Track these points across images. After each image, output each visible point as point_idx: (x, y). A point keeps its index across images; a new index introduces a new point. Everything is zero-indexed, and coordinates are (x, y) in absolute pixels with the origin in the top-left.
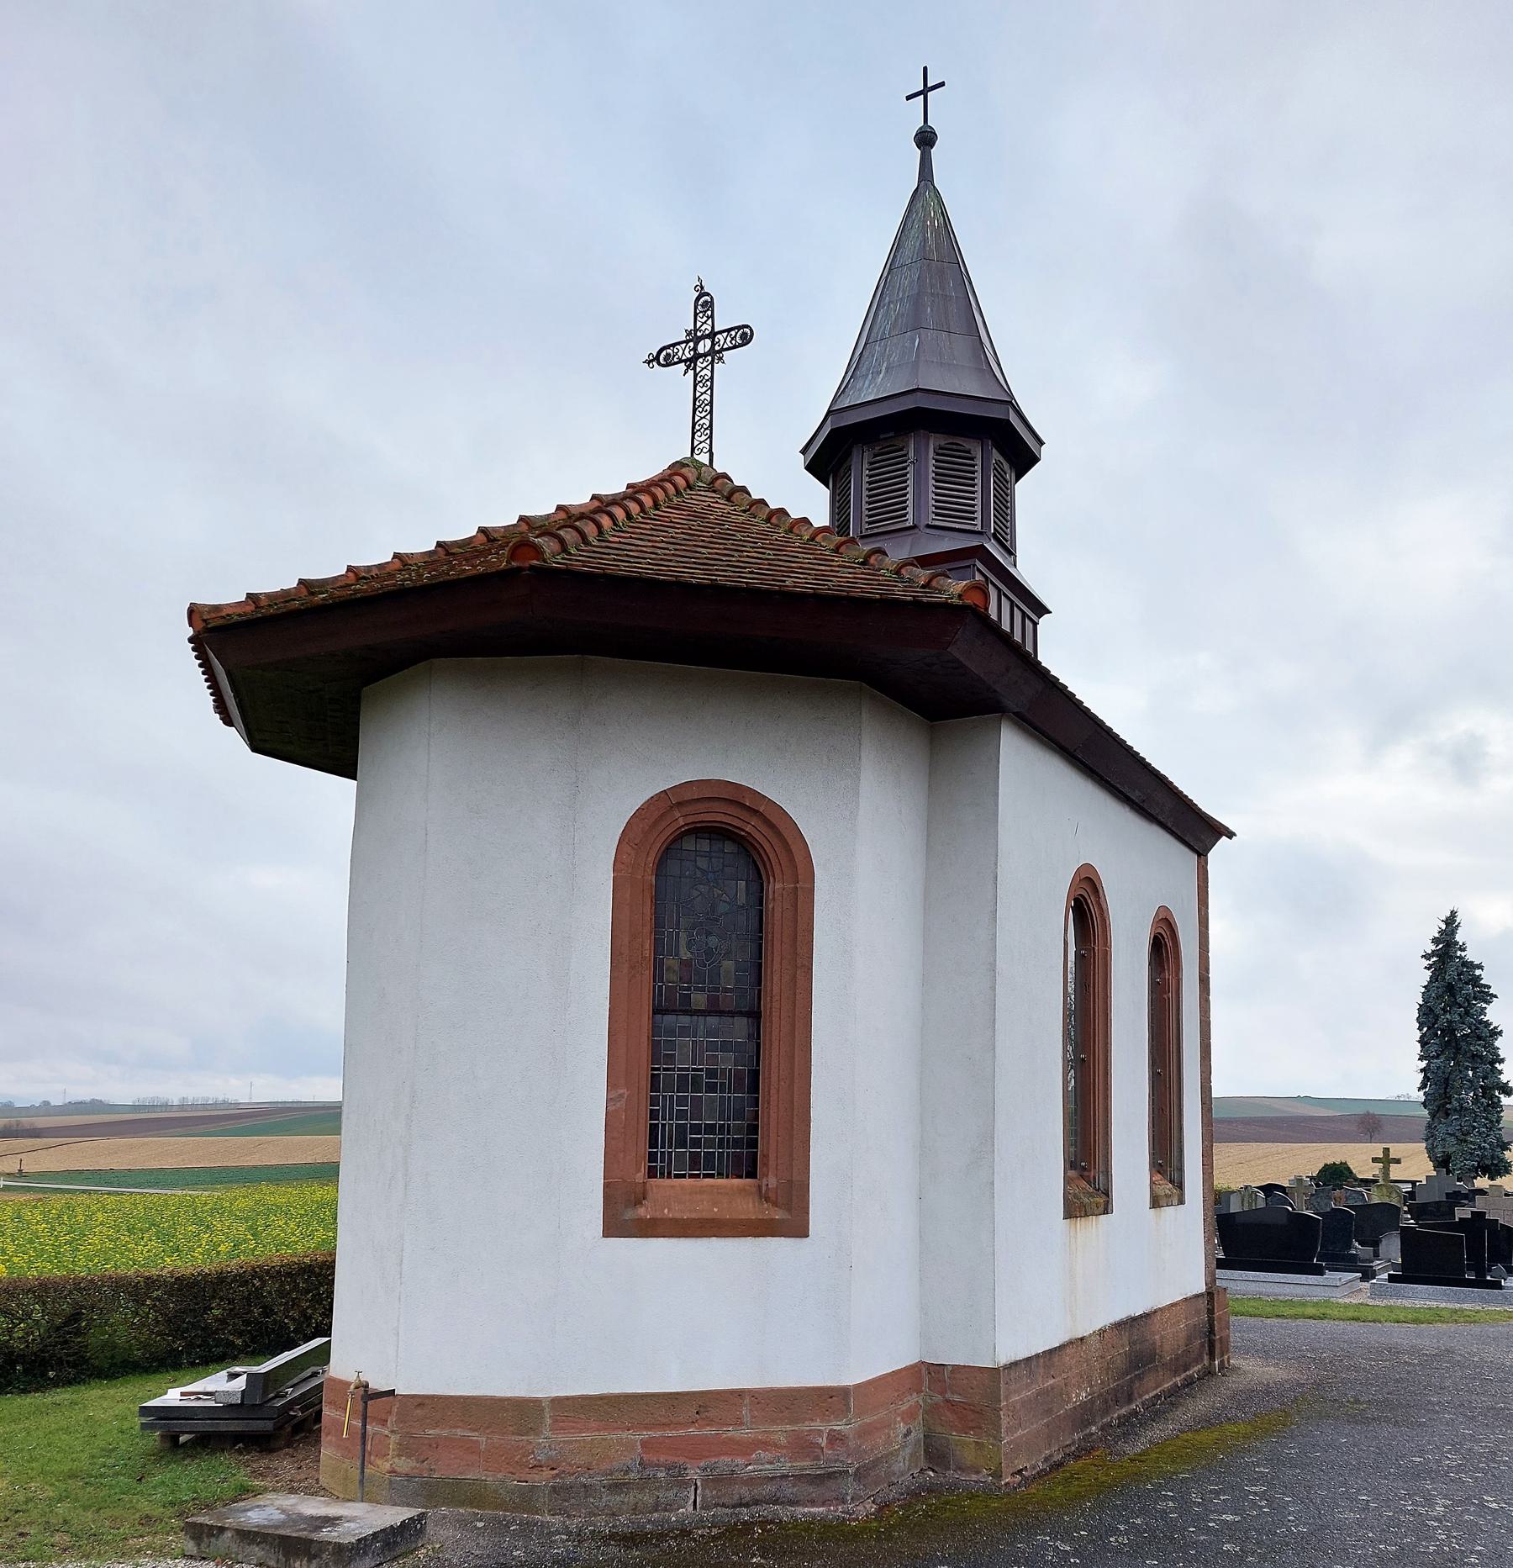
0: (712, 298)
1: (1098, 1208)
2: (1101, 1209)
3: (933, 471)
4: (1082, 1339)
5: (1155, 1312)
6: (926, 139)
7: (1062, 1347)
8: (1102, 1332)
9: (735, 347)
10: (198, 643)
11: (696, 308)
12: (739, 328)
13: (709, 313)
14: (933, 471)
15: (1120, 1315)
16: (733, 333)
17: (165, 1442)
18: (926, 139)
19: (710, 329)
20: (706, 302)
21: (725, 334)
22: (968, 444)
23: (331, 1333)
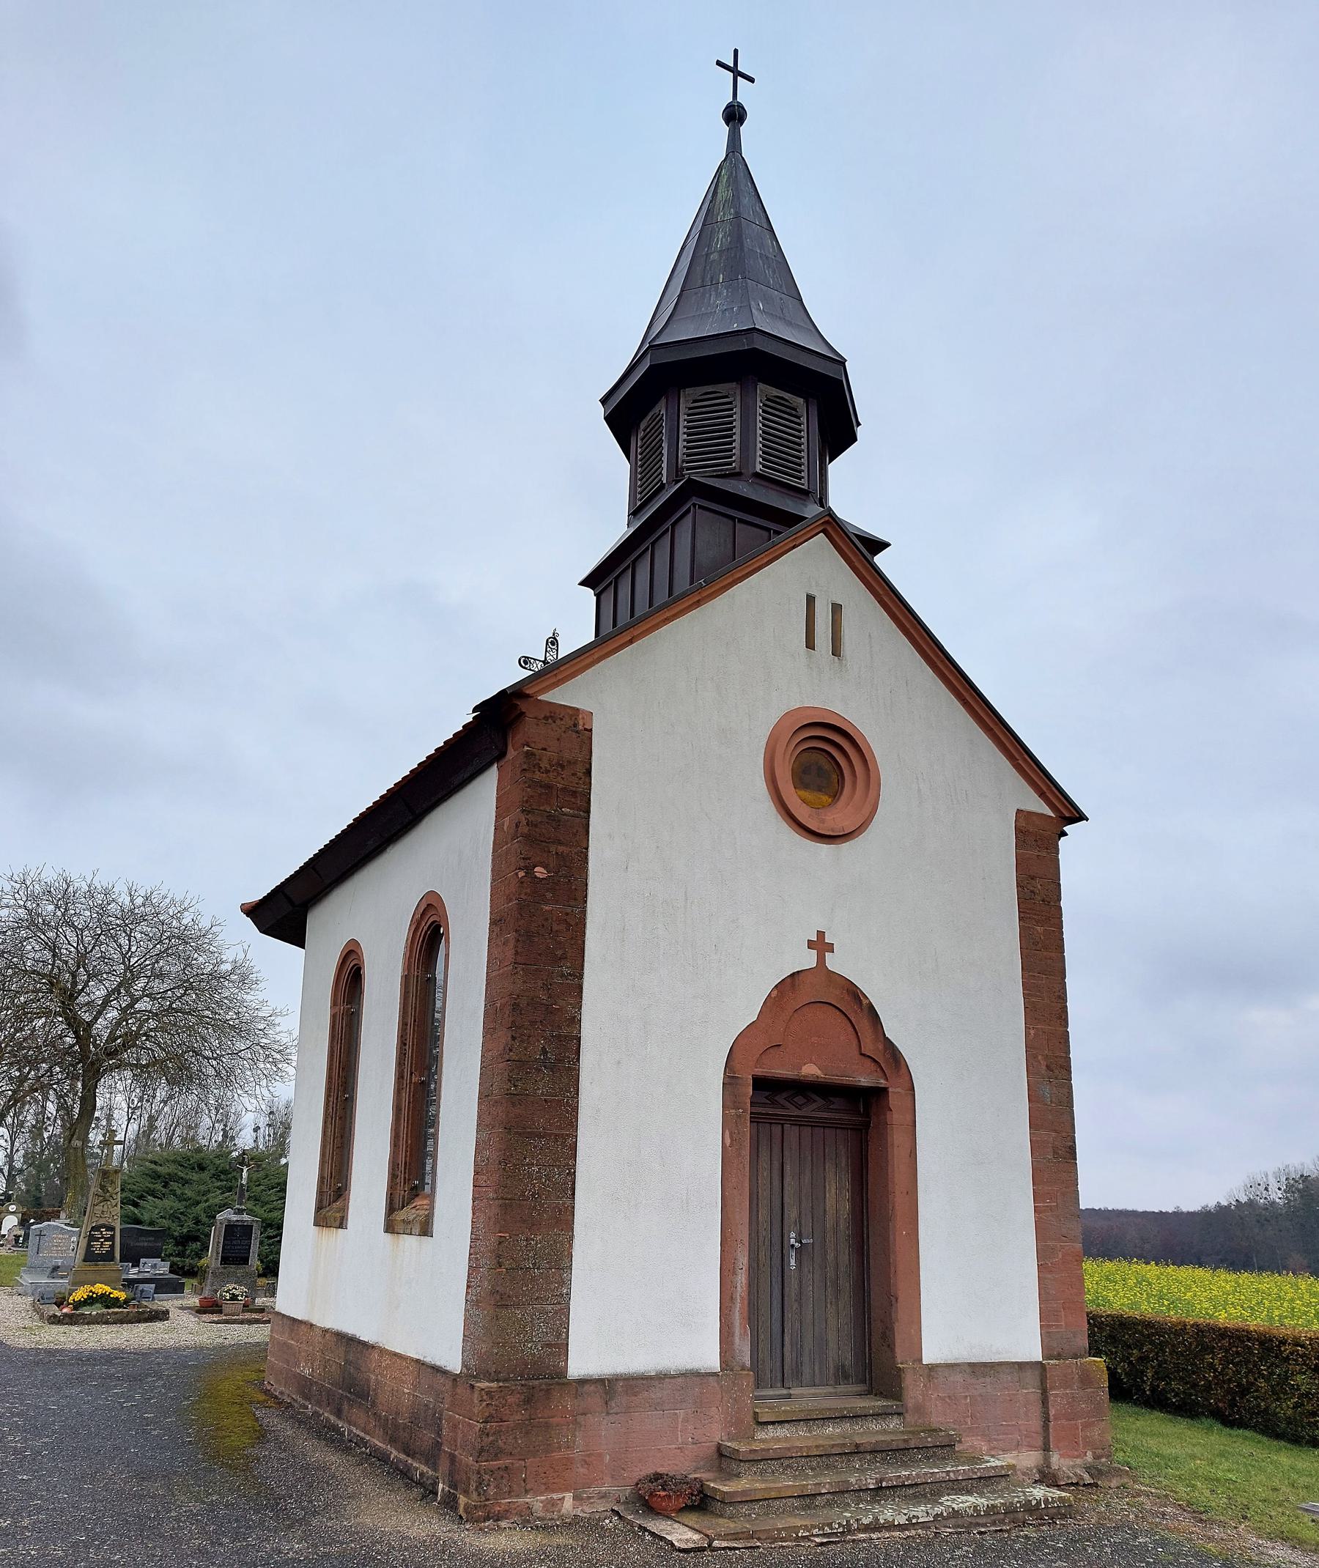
0: (523, 657)
1: (335, 1221)
2: (337, 1223)
3: (760, 449)
4: (312, 1325)
5: (373, 1347)
6: (734, 115)
7: (301, 1322)
8: (326, 1331)
9: (557, 650)
10: (1019, 831)
11: (526, 668)
12: (547, 644)
13: (532, 661)
14: (760, 449)
15: (349, 1328)
16: (548, 649)
17: (1290, 1188)
18: (734, 115)
19: (541, 663)
20: (524, 661)
21: (548, 654)
22: (723, 388)
23: (344, 1210)
